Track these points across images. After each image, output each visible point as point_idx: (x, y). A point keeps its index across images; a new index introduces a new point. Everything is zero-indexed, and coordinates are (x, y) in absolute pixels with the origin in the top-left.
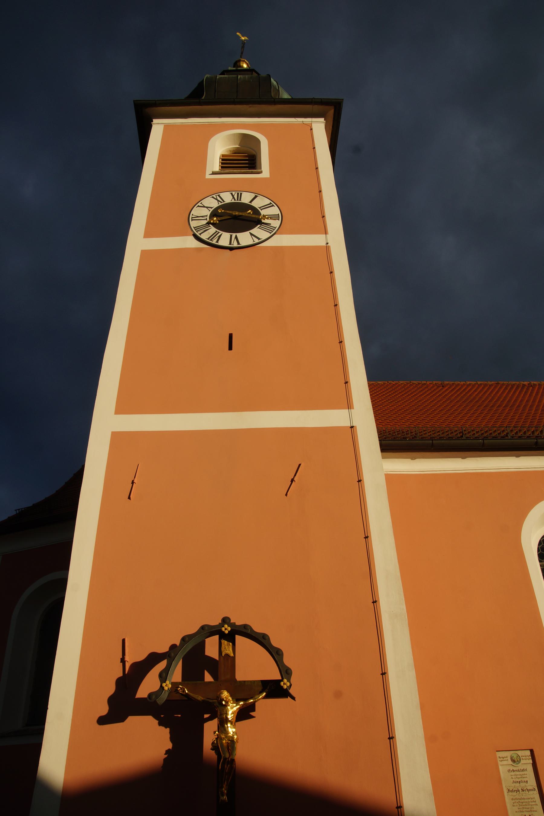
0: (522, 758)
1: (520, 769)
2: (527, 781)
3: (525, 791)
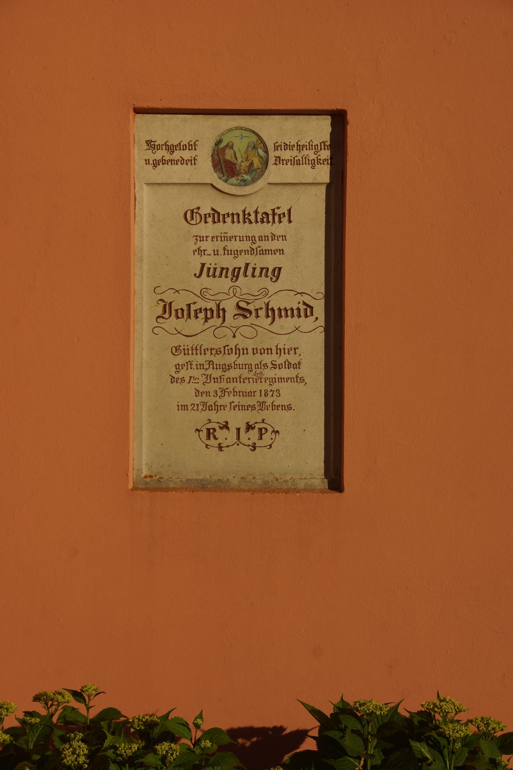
0: (278, 153)
1: (256, 212)
2: (277, 272)
3: (257, 316)
